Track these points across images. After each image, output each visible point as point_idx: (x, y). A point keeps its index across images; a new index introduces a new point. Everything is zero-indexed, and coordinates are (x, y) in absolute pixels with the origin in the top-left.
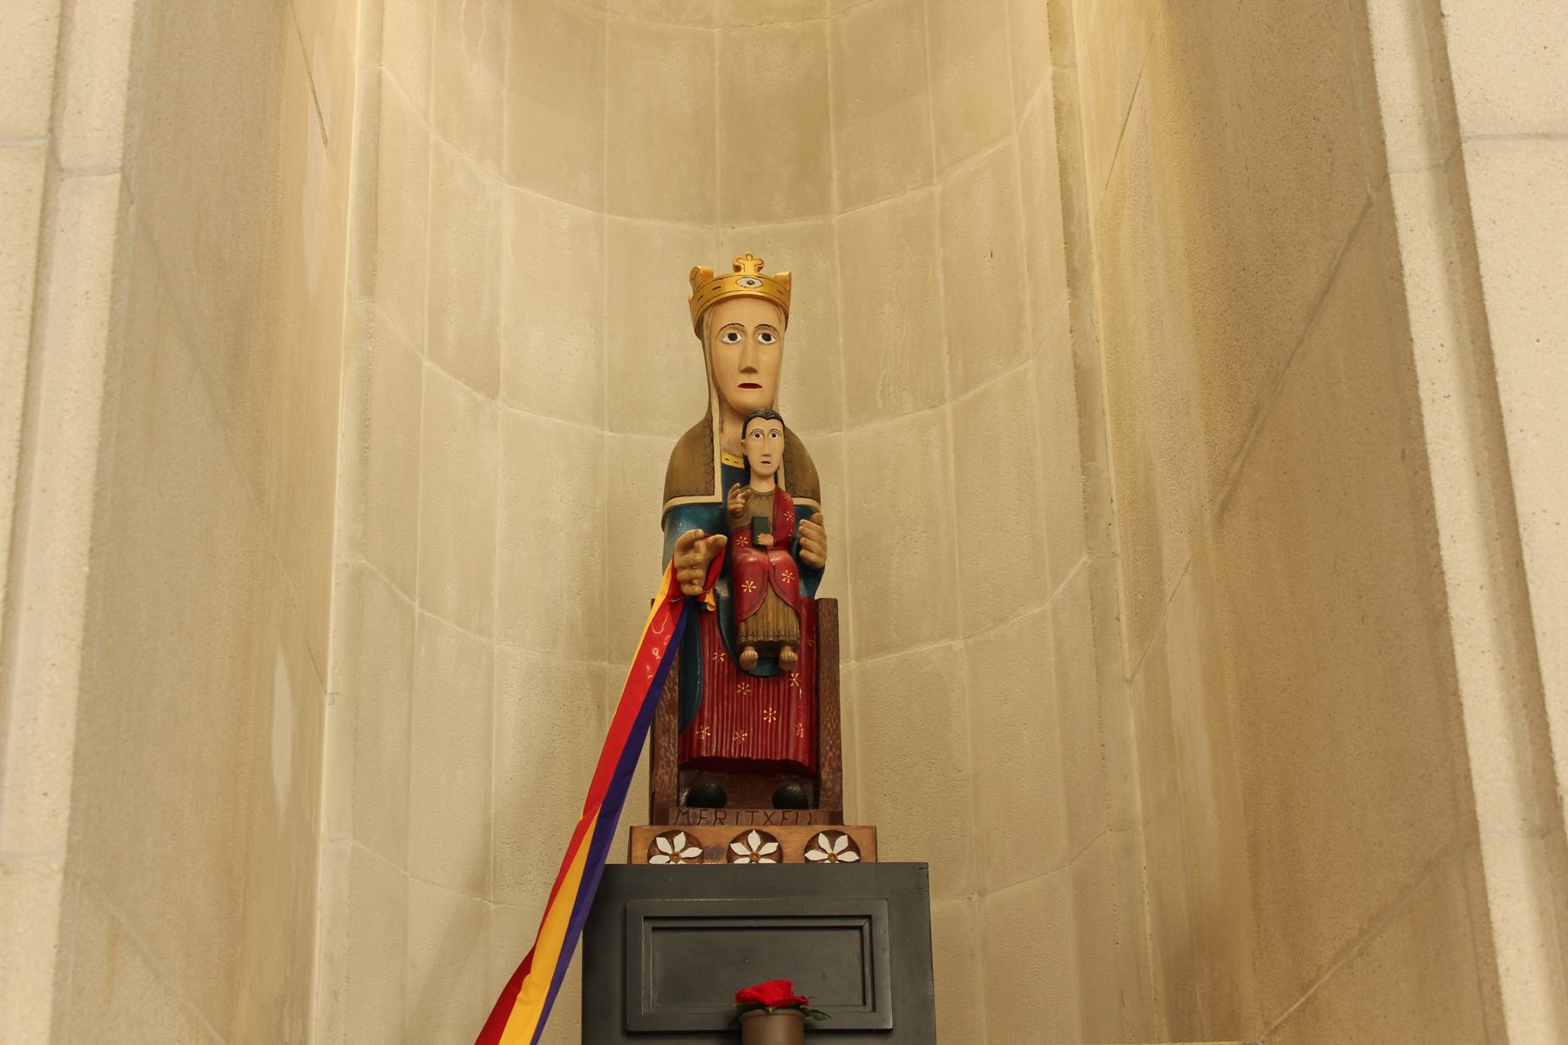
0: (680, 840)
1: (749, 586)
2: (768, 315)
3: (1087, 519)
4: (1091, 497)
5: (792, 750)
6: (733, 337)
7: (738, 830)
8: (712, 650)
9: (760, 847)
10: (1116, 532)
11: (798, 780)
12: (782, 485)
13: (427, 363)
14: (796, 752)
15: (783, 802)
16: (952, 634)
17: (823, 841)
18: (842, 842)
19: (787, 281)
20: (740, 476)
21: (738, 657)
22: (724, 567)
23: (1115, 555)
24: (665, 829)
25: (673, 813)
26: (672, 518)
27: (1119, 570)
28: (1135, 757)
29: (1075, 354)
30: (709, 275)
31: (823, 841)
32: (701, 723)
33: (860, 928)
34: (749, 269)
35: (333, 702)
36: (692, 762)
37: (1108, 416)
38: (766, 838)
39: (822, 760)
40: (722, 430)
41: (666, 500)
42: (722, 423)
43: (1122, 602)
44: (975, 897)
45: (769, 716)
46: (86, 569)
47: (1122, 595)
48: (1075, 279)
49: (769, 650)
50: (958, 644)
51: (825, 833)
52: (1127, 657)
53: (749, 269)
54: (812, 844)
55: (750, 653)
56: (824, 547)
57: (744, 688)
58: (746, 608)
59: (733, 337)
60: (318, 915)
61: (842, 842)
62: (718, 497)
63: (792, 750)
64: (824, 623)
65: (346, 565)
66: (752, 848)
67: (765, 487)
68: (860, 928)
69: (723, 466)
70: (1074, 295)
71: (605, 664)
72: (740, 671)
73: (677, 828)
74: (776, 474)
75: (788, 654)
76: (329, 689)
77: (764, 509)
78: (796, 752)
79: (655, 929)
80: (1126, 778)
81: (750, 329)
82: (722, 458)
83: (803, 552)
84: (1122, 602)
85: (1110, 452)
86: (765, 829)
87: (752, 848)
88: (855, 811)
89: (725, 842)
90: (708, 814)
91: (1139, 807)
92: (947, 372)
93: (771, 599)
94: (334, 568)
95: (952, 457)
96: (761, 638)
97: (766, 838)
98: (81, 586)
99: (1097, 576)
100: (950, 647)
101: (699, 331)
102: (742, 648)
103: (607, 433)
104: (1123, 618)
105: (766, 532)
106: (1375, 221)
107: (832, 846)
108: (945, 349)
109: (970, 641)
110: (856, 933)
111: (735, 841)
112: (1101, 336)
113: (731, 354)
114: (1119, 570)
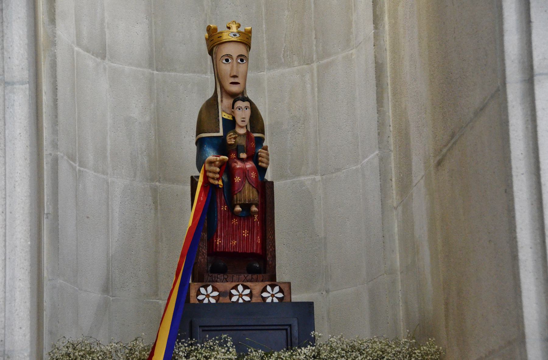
0: (210, 289)
1: (237, 179)
2: (241, 49)
3: (379, 134)
4: (381, 124)
5: (255, 248)
6: (227, 60)
7: (234, 284)
8: (221, 205)
9: (243, 292)
10: (392, 140)
11: (259, 263)
12: (249, 130)
13: (76, 49)
14: (257, 249)
15: (251, 271)
16: (315, 173)
17: (269, 288)
18: (277, 289)
19: (250, 32)
20: (230, 125)
21: (234, 209)
22: (227, 169)
23: (391, 151)
24: (204, 284)
25: (206, 277)
26: (200, 143)
27: (392, 157)
28: (397, 245)
29: (376, 57)
30: (215, 29)
31: (269, 288)
32: (217, 237)
33: (286, 330)
34: (234, 29)
35: (47, 218)
36: (212, 252)
37: (389, 87)
38: (245, 287)
39: (268, 252)
40: (222, 101)
41: (197, 135)
42: (222, 97)
43: (393, 172)
44: (324, 293)
45: (245, 234)
46: (29, 243)
47: (393, 169)
48: (377, 20)
49: (246, 207)
50: (318, 178)
51: (269, 285)
52: (395, 197)
53: (234, 29)
54: (264, 290)
55: (238, 208)
56: (268, 159)
57: (235, 221)
58: (236, 189)
59: (227, 60)
60: (45, 313)
61: (277, 289)
62: (221, 133)
63: (255, 248)
64: (268, 191)
65: (51, 154)
66: (240, 294)
67: (242, 131)
68: (286, 330)
69: (223, 118)
70: (376, 28)
71: (157, 183)
72: (235, 215)
73: (209, 283)
74: (246, 126)
75: (254, 209)
76: (46, 212)
77: (242, 142)
78: (256, 248)
79: (203, 331)
80: (393, 251)
81: (235, 57)
82: (223, 115)
83: (260, 164)
84: (393, 172)
85: (390, 103)
86: (245, 284)
87: (240, 294)
88: (281, 276)
89: (228, 289)
90: (221, 276)
91: (398, 264)
92: (315, 48)
93: (247, 185)
94: (45, 155)
95: (316, 89)
96: (243, 202)
97: (245, 287)
98: (28, 250)
99: (383, 160)
100: (314, 179)
101: (211, 52)
102: (234, 206)
103: (155, 72)
104: (394, 179)
105: (243, 152)
106: (500, 93)
107: (273, 291)
108: (314, 36)
109: (324, 177)
110: (284, 332)
111: (232, 289)
112: (388, 48)
113: (226, 68)
114: (392, 157)
